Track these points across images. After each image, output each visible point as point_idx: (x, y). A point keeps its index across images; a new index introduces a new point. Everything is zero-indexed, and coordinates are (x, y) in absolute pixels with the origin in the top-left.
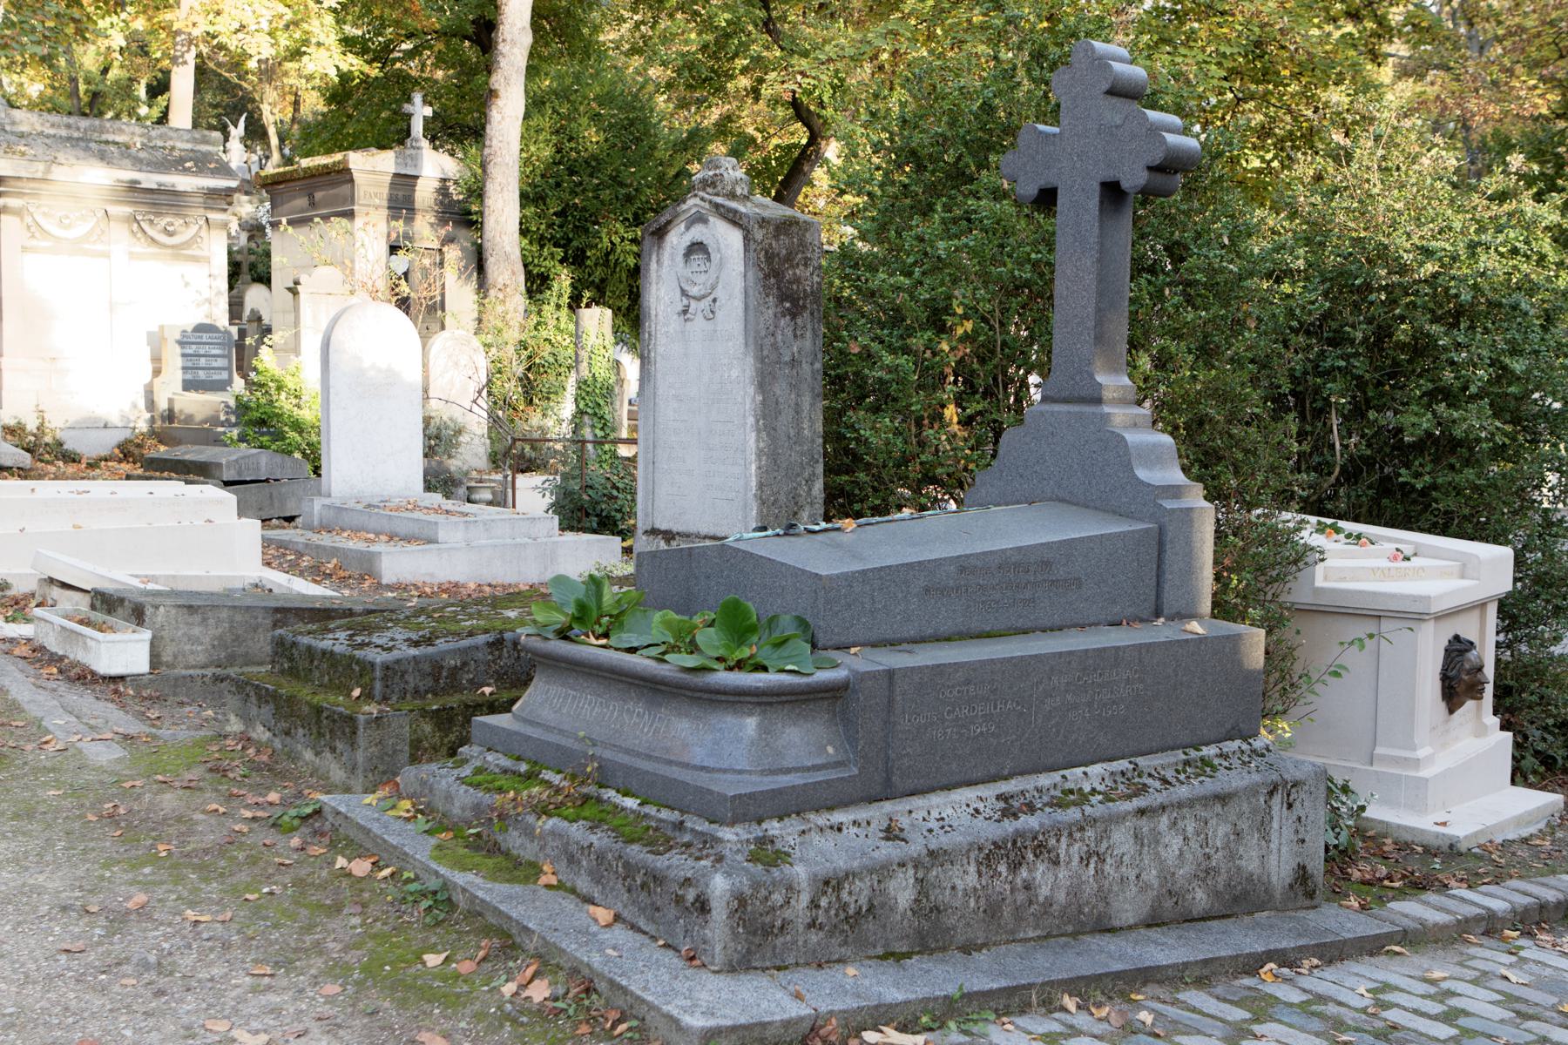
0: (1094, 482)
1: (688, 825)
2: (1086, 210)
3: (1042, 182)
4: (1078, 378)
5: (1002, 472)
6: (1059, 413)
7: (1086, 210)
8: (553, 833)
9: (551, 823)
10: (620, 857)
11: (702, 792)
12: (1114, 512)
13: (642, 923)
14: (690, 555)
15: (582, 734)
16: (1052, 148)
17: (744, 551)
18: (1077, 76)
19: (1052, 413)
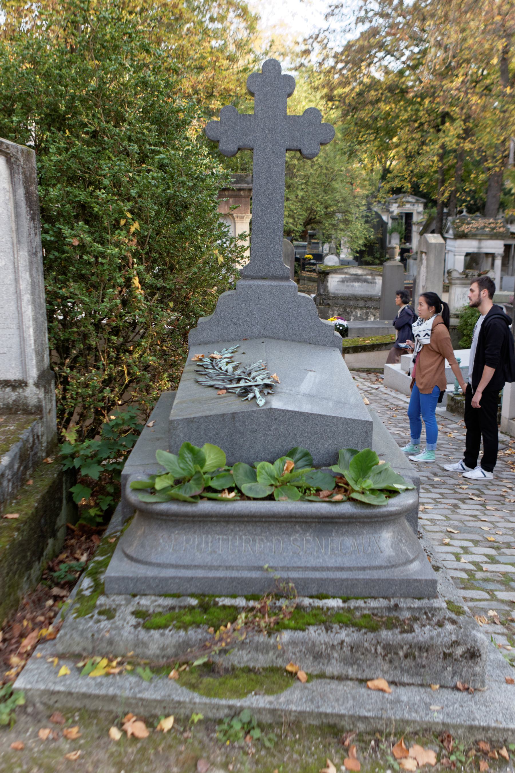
0: (290, 325)
1: (402, 605)
2: (276, 165)
3: (241, 144)
4: (271, 265)
5: (219, 322)
6: (263, 286)
7: (276, 165)
8: (293, 643)
9: (286, 636)
10: (378, 643)
11: (390, 582)
12: (305, 342)
13: (406, 679)
14: (234, 418)
15: (266, 566)
16: (248, 123)
17: (292, 412)
18: (268, 80)
19: (258, 286)
